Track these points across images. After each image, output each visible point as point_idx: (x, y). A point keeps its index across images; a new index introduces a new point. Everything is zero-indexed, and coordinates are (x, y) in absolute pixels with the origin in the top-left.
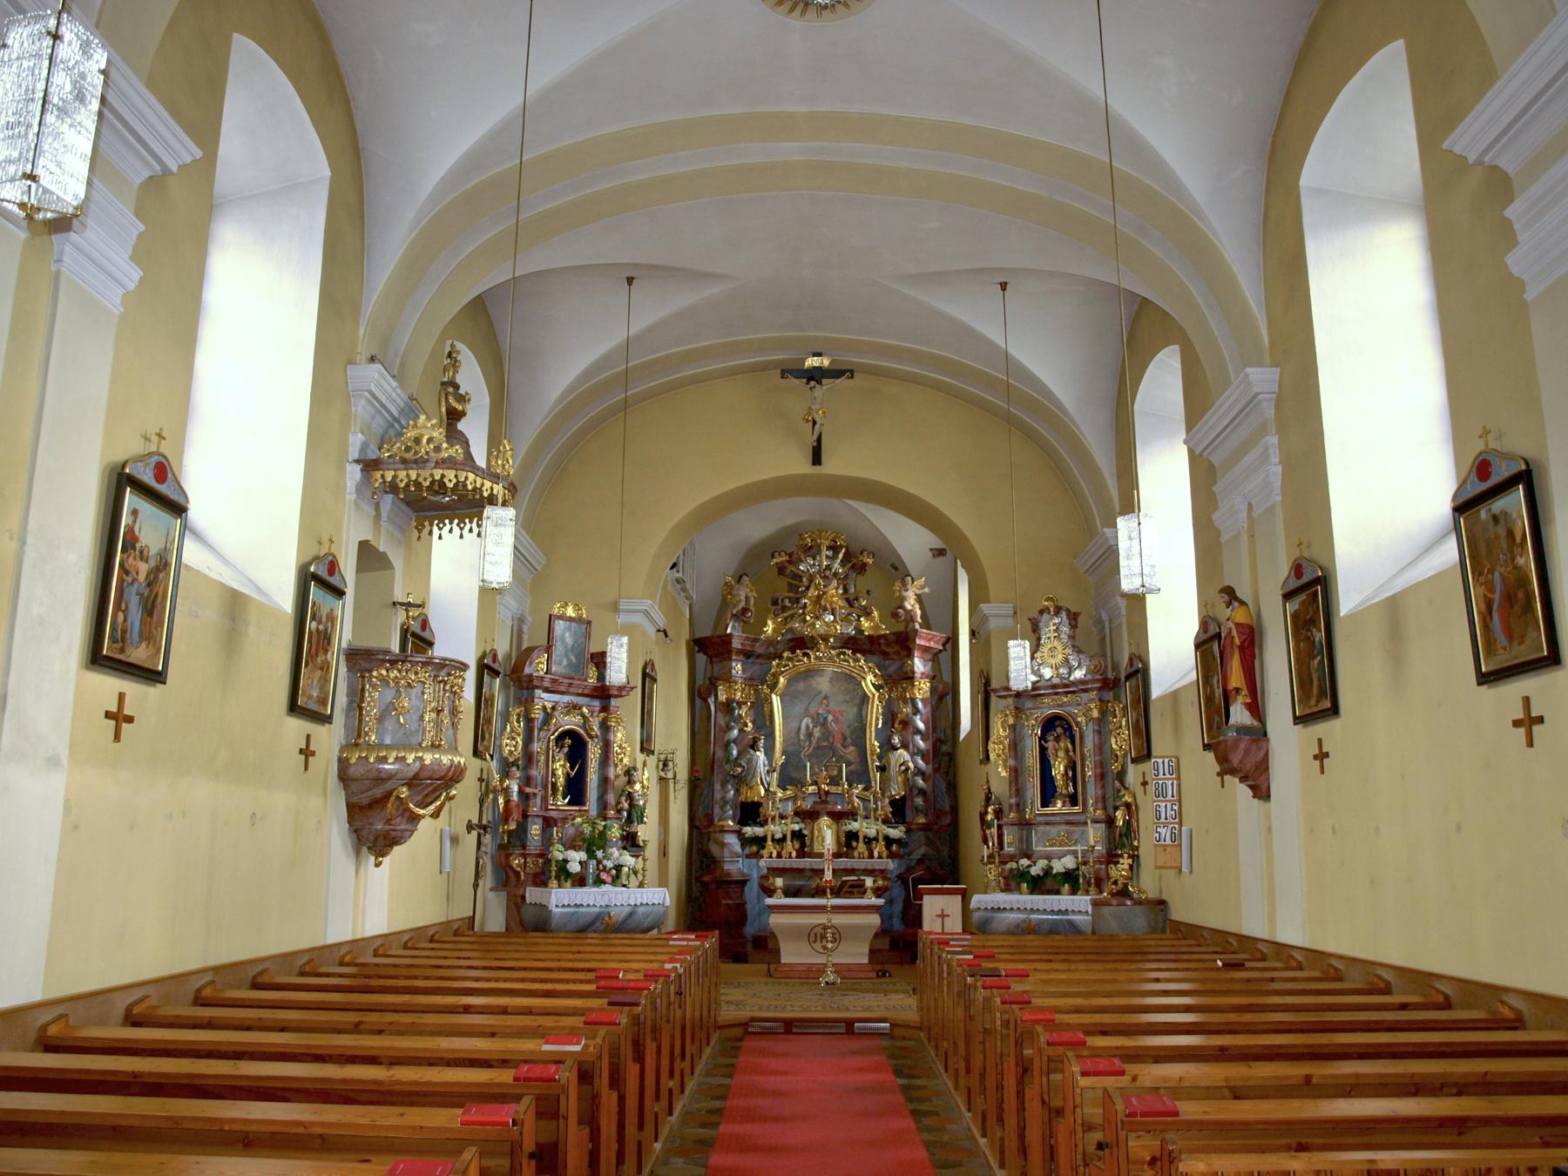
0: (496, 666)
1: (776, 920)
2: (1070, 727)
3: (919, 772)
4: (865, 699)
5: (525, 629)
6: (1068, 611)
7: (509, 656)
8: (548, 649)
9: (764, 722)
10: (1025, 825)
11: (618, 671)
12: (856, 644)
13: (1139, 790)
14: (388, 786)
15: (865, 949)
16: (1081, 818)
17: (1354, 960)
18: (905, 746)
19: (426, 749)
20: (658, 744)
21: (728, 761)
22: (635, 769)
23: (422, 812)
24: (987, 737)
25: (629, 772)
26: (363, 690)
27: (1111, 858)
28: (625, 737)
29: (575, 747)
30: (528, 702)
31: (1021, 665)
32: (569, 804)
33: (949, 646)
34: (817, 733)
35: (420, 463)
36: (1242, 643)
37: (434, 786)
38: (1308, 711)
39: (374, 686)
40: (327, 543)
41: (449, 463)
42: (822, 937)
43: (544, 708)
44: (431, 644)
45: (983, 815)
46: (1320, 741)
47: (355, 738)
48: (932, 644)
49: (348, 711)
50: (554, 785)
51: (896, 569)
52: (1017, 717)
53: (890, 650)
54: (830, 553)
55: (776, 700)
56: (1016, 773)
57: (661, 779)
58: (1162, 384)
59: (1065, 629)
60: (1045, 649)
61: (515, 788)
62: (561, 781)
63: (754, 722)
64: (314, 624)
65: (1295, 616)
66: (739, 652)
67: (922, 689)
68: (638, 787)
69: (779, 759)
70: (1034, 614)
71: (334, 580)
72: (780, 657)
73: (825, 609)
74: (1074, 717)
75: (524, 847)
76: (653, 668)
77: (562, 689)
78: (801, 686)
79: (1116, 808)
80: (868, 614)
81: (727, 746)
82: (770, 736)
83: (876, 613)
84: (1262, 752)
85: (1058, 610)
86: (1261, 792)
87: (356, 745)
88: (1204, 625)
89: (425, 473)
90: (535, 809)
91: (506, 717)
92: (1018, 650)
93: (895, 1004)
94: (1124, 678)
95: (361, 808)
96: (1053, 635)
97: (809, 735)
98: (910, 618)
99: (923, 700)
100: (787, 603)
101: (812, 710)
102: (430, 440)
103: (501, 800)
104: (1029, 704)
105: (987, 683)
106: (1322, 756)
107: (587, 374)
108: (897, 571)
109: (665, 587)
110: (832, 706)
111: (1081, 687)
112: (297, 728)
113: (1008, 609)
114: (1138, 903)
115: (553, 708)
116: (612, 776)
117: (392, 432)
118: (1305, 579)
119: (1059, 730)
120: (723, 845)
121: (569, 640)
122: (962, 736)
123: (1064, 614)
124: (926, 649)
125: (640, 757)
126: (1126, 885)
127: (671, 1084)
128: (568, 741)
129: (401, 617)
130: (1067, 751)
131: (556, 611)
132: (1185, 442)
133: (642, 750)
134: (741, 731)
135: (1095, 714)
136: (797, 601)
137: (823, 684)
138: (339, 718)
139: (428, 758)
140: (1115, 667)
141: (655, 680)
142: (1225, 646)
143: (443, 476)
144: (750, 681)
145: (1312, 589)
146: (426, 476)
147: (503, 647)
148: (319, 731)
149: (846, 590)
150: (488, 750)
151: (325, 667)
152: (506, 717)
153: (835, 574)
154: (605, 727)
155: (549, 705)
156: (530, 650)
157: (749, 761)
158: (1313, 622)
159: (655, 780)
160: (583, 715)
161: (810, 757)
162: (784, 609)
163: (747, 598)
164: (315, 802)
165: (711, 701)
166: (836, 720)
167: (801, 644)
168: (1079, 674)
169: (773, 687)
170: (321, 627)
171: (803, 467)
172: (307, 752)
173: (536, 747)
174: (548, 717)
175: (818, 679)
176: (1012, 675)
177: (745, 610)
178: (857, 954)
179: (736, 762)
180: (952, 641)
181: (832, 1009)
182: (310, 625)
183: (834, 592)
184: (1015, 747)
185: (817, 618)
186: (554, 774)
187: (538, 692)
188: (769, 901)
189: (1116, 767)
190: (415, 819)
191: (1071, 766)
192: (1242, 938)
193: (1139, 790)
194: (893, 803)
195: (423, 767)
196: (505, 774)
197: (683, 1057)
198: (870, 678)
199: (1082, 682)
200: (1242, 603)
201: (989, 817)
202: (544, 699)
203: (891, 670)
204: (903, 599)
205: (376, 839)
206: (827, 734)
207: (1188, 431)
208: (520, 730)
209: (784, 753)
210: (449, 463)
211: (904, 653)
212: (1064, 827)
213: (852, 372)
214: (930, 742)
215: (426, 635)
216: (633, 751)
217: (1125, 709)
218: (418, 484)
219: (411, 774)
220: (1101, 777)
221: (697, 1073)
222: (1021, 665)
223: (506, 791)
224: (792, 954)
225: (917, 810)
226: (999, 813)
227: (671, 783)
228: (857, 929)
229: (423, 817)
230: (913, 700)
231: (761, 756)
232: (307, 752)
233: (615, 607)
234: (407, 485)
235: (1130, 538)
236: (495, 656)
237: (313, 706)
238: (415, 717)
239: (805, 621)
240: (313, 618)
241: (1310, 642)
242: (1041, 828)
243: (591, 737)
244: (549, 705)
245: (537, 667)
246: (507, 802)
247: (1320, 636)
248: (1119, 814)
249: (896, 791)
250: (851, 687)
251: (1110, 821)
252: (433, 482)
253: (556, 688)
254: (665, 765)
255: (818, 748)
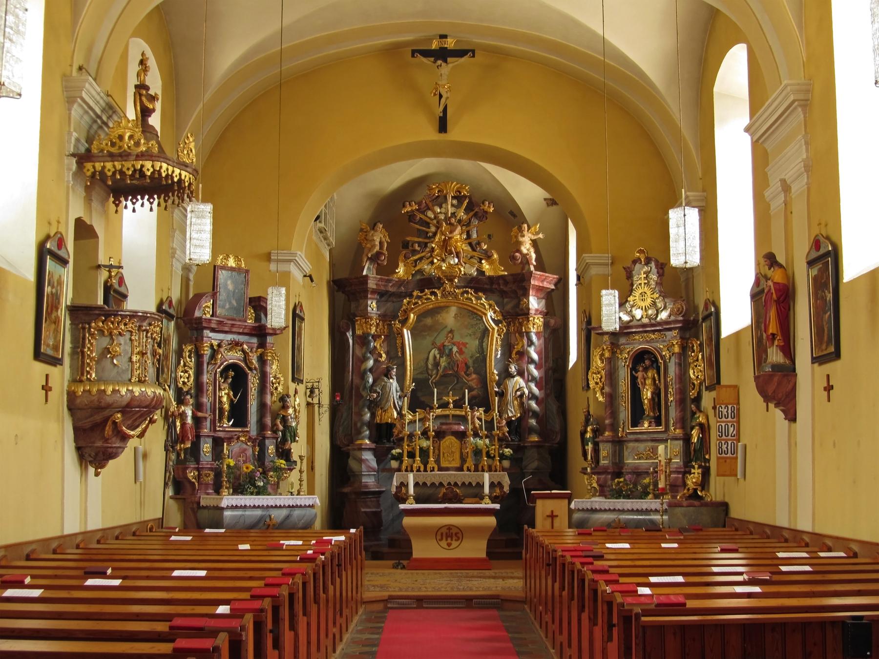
0: (171, 311)
1: (407, 521)
2: (657, 360)
3: (533, 396)
4: (486, 332)
5: (191, 277)
6: (657, 262)
7: (180, 302)
8: (214, 295)
9: (396, 354)
10: (619, 443)
11: (277, 315)
12: (479, 284)
13: (711, 413)
14: (107, 413)
15: (483, 544)
16: (664, 436)
17: (837, 538)
18: (521, 373)
19: (135, 384)
20: (307, 374)
21: (365, 387)
22: (288, 396)
23: (132, 433)
24: (588, 368)
25: (283, 399)
26: (84, 338)
27: (686, 470)
28: (277, 369)
29: (237, 377)
30: (198, 341)
31: (611, 313)
32: (233, 426)
33: (560, 286)
34: (443, 362)
35: (124, 156)
36: (779, 298)
37: (138, 412)
38: (821, 354)
39: (92, 335)
40: (55, 224)
41: (146, 156)
42: (448, 542)
43: (212, 346)
44: (125, 296)
45: (583, 433)
46: (828, 376)
47: (79, 375)
48: (545, 284)
49: (74, 353)
50: (221, 410)
51: (514, 216)
52: (613, 353)
53: (509, 290)
54: (455, 202)
55: (407, 334)
56: (612, 399)
57: (308, 404)
58: (734, 70)
59: (654, 277)
60: (637, 294)
61: (189, 413)
62: (226, 407)
63: (387, 353)
64: (50, 288)
65: (815, 279)
66: (374, 292)
67: (536, 324)
68: (291, 411)
69: (410, 385)
70: (628, 264)
71: (62, 253)
72: (411, 296)
73: (451, 253)
74: (659, 351)
75: (197, 461)
76: (301, 310)
77: (226, 329)
78: (429, 321)
79: (692, 428)
80: (489, 257)
81: (363, 376)
82: (402, 365)
83: (495, 256)
84: (790, 386)
85: (648, 261)
86: (791, 417)
87: (81, 381)
88: (757, 282)
89: (128, 164)
90: (206, 431)
91: (180, 354)
92: (609, 298)
93: (508, 582)
94: (696, 318)
95: (85, 430)
96: (643, 281)
97: (437, 364)
98: (526, 260)
99: (537, 334)
100: (417, 247)
101: (438, 343)
102: (131, 137)
103: (178, 424)
104: (622, 340)
105: (589, 322)
106: (829, 388)
107: (245, 58)
108: (511, 217)
109: (310, 239)
110: (457, 339)
111: (663, 327)
112: (41, 368)
113: (606, 258)
114: (707, 505)
115: (219, 346)
116: (269, 402)
117: (95, 127)
118: (822, 251)
119: (647, 362)
120: (361, 461)
121: (230, 287)
122: (571, 365)
123: (653, 265)
124: (539, 289)
125: (292, 386)
126: (695, 490)
127: (334, 630)
128: (232, 373)
129: (104, 275)
130: (654, 379)
131: (219, 263)
132: (747, 130)
133: (294, 380)
134: (376, 361)
135: (677, 349)
136: (426, 245)
137: (449, 318)
138: (67, 361)
139: (137, 390)
140: (696, 308)
141: (303, 319)
142: (773, 298)
143: (142, 166)
144: (386, 318)
145: (827, 257)
146: (128, 167)
147: (176, 294)
148: (54, 371)
149: (469, 236)
150: (166, 381)
151: (57, 322)
152: (180, 354)
153: (460, 221)
154: (262, 360)
155: (215, 343)
156: (198, 297)
157: (384, 388)
158: (825, 285)
159: (304, 405)
160: (243, 351)
161: (437, 384)
162: (414, 252)
163: (381, 243)
164: (53, 427)
165: (349, 334)
166: (461, 352)
167: (428, 283)
168: (664, 315)
169: (404, 322)
170: (54, 290)
171: (431, 134)
172: (46, 388)
173: (205, 378)
174: (214, 353)
175: (444, 315)
176: (604, 319)
177: (379, 254)
178: (476, 549)
179: (372, 389)
180: (563, 282)
181: (459, 590)
182: (47, 290)
183: (458, 235)
184: (611, 376)
185: (443, 260)
186: (221, 402)
187: (207, 333)
188: (402, 506)
189: (693, 394)
190: (125, 438)
191: (656, 393)
192: (774, 528)
193: (711, 413)
194: (509, 423)
195: (133, 398)
196: (180, 401)
197: (341, 615)
198: (490, 314)
199: (666, 322)
200: (780, 266)
201: (588, 435)
202: (212, 338)
203: (508, 307)
204: (520, 244)
205: (97, 454)
206: (452, 363)
207: (752, 113)
208: (192, 364)
209: (414, 380)
210: (146, 156)
211: (520, 292)
212: (650, 444)
213: (473, 51)
214: (543, 370)
215: (122, 289)
216: (286, 380)
217: (701, 345)
218: (122, 172)
219: (124, 403)
220: (682, 401)
221: (350, 630)
222: (611, 313)
223: (183, 416)
224: (421, 549)
225: (531, 430)
226: (596, 432)
227: (316, 407)
228: (476, 531)
229: (133, 437)
230: (528, 333)
231: (394, 383)
232: (46, 388)
233: (268, 257)
234: (114, 173)
235: (678, 227)
236: (171, 302)
237: (50, 352)
238: (126, 359)
239: (432, 263)
240: (49, 285)
241: (824, 299)
242: (631, 445)
243: (250, 369)
244: (215, 343)
245: (205, 310)
246: (183, 425)
247: (830, 296)
248: (695, 432)
249: (513, 412)
250: (474, 322)
251: (687, 439)
252: (135, 170)
253: (222, 328)
254: (312, 392)
255: (444, 376)
